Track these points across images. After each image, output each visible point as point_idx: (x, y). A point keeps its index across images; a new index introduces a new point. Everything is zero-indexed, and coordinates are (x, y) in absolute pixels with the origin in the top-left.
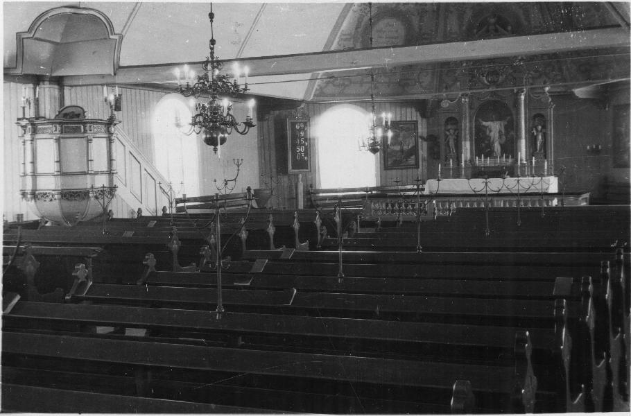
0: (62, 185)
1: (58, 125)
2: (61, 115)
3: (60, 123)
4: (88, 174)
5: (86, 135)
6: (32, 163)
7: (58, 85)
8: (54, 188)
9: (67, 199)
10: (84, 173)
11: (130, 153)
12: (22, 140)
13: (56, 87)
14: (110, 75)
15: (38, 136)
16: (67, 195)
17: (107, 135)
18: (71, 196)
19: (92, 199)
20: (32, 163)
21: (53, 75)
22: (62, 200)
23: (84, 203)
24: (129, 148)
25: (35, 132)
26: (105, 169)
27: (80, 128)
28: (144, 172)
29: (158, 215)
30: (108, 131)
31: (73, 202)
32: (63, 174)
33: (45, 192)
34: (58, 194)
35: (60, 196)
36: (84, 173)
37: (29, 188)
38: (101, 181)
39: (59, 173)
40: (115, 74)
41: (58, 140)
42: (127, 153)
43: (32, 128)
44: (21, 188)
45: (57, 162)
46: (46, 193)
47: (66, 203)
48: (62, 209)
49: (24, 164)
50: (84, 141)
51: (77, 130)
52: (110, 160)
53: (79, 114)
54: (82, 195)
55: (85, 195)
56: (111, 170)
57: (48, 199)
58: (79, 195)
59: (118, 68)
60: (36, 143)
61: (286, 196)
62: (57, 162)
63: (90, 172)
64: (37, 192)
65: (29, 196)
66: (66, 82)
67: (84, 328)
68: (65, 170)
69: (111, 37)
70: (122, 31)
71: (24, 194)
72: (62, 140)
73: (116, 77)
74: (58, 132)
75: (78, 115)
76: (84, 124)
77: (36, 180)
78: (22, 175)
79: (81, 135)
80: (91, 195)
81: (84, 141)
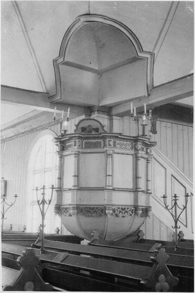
1: (77, 140)
2: (80, 131)
3: (79, 138)
4: (106, 189)
5: (105, 149)
6: (58, 178)
7: (109, 115)
10: (102, 189)
11: (172, 175)
13: (106, 117)
14: (145, 96)
15: (66, 153)
16: (83, 210)
17: (133, 152)
18: (88, 211)
19: (109, 216)
20: (58, 178)
21: (100, 105)
23: (102, 219)
24: (170, 171)
26: (130, 186)
30: (135, 149)
32: (79, 188)
34: (73, 209)
35: (76, 211)
36: (102, 189)
38: (124, 199)
39: (77, 188)
40: (149, 95)
42: (169, 176)
47: (84, 219)
48: (80, 225)
51: (96, 145)
52: (136, 178)
54: (99, 211)
55: (102, 212)
58: (95, 211)
59: (151, 89)
60: (64, 159)
61: (106, 199)
62: (74, 176)
63: (107, 188)
66: (114, 112)
68: (83, 185)
69: (140, 54)
70: (154, 50)
72: (81, 155)
73: (150, 97)
74: (76, 147)
75: (97, 130)
76: (104, 138)
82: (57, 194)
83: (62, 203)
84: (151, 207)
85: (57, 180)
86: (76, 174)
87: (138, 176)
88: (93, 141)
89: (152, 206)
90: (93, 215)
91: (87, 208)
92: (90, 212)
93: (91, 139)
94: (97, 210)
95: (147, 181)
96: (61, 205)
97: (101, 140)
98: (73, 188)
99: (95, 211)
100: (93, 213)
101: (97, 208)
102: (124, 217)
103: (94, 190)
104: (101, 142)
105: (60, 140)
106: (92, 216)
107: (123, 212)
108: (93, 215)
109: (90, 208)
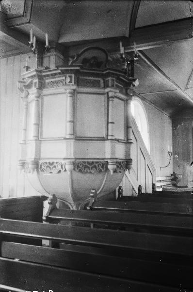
0: (75, 152)
4: (107, 139)
5: (107, 90)
6: (35, 124)
8: (64, 156)
9: (80, 171)
10: (103, 139)
12: (25, 103)
15: (45, 91)
18: (86, 167)
20: (35, 124)
21: (60, 41)
22: (73, 172)
25: (41, 86)
27: (99, 82)
28: (139, 150)
29: (148, 192)
31: (88, 175)
33: (51, 161)
37: (30, 157)
41: (74, 93)
43: (39, 82)
44: (20, 158)
45: (70, 121)
46: (53, 163)
47: (78, 175)
49: (25, 130)
50: (103, 98)
53: (102, 63)
54: (100, 166)
56: (128, 139)
57: (55, 171)
58: (95, 167)
62: (70, 121)
63: (109, 138)
64: (41, 162)
65: (30, 166)
67: (38, 242)
68: (79, 134)
71: (23, 164)
77: (36, 152)
78: (23, 142)
79: (101, 91)
80: (110, 167)
81: (103, 98)
82: (36, 145)
83: (40, 157)
84: (131, 160)
85: (69, 124)
86: (72, 120)
87: (37, 126)
88: (89, 78)
89: (133, 159)
90: (92, 171)
91: (85, 162)
92: (89, 168)
93: (86, 76)
94: (97, 165)
95: (25, 130)
96: (40, 159)
97: (100, 79)
98: (68, 137)
99: (95, 167)
100: (92, 168)
101: (97, 162)
102: (51, 173)
103: (95, 140)
104: (100, 81)
105: (40, 74)
106: (91, 173)
107: (90, 167)
108: (92, 171)
109: (88, 163)
